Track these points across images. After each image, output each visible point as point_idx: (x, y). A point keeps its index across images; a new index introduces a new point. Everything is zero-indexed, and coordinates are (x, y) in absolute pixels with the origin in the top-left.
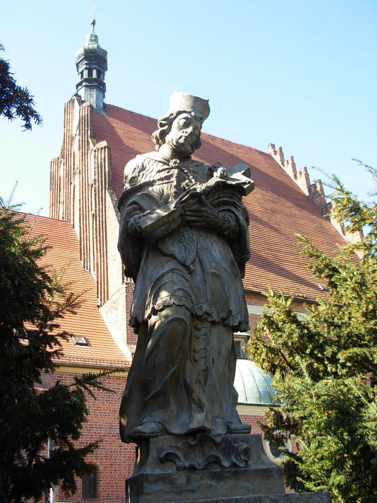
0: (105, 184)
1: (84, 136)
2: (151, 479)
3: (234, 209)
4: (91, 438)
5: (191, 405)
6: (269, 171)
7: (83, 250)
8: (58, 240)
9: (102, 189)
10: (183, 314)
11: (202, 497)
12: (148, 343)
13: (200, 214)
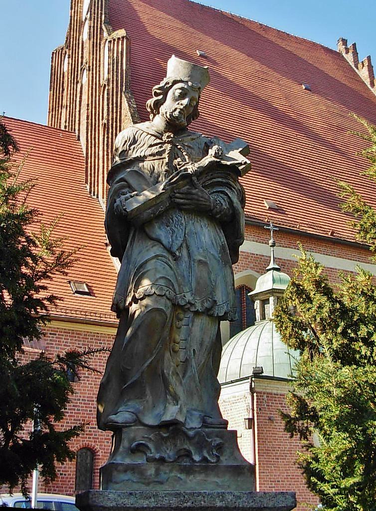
0: (122, 86)
1: (96, 21)
2: (120, 468)
4: (89, 414)
5: (167, 397)
6: (338, 75)
7: (89, 170)
8: (53, 163)
9: (117, 92)
10: (163, 304)
11: (170, 490)
12: (127, 333)
13: (190, 197)
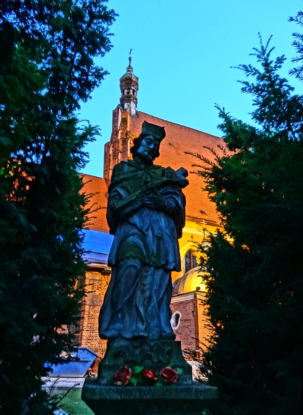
3: (175, 196)
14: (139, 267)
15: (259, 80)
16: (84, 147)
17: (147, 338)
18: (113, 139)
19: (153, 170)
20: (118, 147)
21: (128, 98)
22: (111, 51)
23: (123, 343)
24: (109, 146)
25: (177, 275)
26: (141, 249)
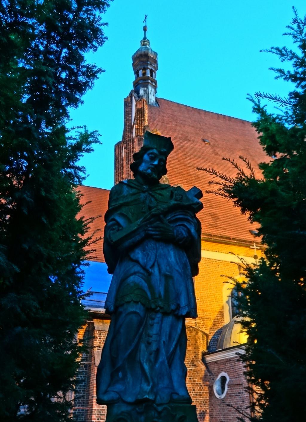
3: (186, 224)
14: (142, 314)
15: (296, 67)
16: (79, 160)
17: (154, 401)
18: (126, 138)
19: (158, 192)
20: (133, 148)
21: (144, 82)
22: (105, 45)
23: (124, 408)
24: (121, 147)
25: (220, 322)
26: (144, 291)
